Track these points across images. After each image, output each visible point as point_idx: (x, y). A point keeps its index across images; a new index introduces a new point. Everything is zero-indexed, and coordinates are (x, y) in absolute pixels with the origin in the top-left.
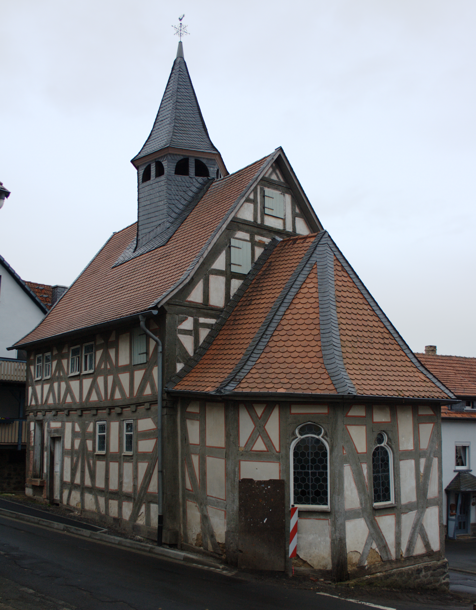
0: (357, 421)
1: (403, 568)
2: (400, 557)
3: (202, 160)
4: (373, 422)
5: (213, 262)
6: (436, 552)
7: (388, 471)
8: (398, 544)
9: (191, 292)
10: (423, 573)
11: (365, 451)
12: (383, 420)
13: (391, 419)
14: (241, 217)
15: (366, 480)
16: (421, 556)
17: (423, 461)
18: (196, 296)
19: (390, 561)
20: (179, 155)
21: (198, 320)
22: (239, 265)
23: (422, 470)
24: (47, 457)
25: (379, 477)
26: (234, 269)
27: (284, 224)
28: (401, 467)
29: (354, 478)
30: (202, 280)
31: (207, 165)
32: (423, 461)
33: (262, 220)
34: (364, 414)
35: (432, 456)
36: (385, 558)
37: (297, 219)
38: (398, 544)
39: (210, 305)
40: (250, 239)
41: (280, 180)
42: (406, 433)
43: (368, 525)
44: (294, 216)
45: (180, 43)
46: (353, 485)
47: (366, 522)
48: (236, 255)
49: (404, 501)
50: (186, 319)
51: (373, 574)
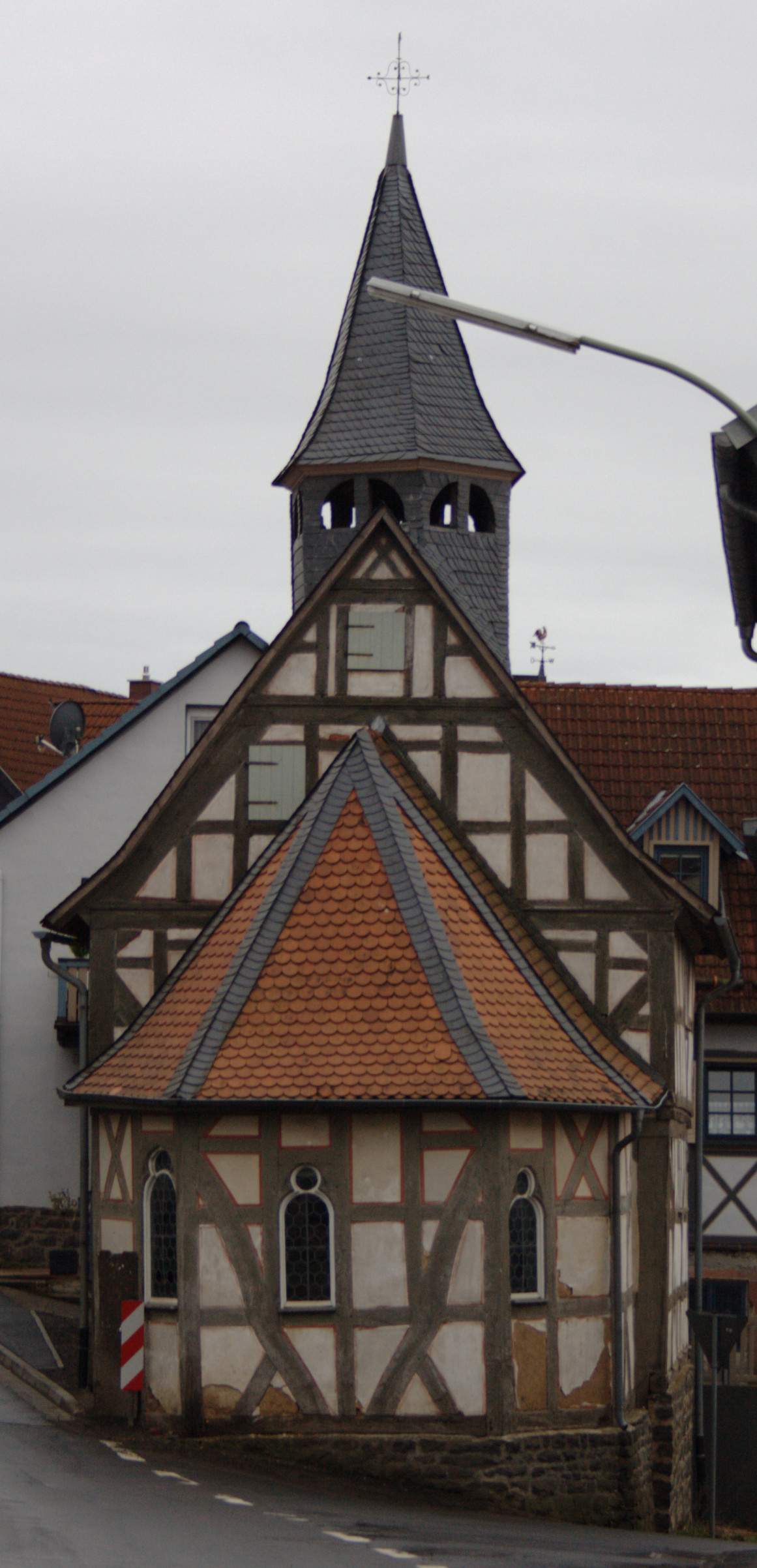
1: (361, 1436)
2: (354, 1413)
3: (385, 479)
4: (281, 1148)
5: (203, 806)
7: (326, 1241)
8: (346, 1385)
10: (418, 1452)
11: (255, 1200)
12: (309, 1143)
13: (544, 1142)
15: (260, 1257)
16: (421, 1421)
17: (430, 1230)
18: (160, 883)
19: (323, 1418)
20: (331, 476)
21: (165, 935)
22: (270, 803)
23: (427, 1244)
24: (627, 1334)
25: (304, 1254)
26: (256, 813)
27: (408, 682)
28: (353, 1236)
29: (227, 1251)
31: (398, 490)
32: (430, 1230)
33: (342, 684)
34: (253, 1131)
36: (309, 1408)
37: (450, 661)
38: (346, 1385)
39: (194, 901)
40: (306, 736)
41: (400, 574)
42: (375, 1169)
43: (261, 1341)
44: (441, 654)
45: (398, 118)
46: (225, 1263)
47: (257, 1334)
48: (260, 783)
49: (361, 1301)
50: (137, 935)
51: (272, 1433)
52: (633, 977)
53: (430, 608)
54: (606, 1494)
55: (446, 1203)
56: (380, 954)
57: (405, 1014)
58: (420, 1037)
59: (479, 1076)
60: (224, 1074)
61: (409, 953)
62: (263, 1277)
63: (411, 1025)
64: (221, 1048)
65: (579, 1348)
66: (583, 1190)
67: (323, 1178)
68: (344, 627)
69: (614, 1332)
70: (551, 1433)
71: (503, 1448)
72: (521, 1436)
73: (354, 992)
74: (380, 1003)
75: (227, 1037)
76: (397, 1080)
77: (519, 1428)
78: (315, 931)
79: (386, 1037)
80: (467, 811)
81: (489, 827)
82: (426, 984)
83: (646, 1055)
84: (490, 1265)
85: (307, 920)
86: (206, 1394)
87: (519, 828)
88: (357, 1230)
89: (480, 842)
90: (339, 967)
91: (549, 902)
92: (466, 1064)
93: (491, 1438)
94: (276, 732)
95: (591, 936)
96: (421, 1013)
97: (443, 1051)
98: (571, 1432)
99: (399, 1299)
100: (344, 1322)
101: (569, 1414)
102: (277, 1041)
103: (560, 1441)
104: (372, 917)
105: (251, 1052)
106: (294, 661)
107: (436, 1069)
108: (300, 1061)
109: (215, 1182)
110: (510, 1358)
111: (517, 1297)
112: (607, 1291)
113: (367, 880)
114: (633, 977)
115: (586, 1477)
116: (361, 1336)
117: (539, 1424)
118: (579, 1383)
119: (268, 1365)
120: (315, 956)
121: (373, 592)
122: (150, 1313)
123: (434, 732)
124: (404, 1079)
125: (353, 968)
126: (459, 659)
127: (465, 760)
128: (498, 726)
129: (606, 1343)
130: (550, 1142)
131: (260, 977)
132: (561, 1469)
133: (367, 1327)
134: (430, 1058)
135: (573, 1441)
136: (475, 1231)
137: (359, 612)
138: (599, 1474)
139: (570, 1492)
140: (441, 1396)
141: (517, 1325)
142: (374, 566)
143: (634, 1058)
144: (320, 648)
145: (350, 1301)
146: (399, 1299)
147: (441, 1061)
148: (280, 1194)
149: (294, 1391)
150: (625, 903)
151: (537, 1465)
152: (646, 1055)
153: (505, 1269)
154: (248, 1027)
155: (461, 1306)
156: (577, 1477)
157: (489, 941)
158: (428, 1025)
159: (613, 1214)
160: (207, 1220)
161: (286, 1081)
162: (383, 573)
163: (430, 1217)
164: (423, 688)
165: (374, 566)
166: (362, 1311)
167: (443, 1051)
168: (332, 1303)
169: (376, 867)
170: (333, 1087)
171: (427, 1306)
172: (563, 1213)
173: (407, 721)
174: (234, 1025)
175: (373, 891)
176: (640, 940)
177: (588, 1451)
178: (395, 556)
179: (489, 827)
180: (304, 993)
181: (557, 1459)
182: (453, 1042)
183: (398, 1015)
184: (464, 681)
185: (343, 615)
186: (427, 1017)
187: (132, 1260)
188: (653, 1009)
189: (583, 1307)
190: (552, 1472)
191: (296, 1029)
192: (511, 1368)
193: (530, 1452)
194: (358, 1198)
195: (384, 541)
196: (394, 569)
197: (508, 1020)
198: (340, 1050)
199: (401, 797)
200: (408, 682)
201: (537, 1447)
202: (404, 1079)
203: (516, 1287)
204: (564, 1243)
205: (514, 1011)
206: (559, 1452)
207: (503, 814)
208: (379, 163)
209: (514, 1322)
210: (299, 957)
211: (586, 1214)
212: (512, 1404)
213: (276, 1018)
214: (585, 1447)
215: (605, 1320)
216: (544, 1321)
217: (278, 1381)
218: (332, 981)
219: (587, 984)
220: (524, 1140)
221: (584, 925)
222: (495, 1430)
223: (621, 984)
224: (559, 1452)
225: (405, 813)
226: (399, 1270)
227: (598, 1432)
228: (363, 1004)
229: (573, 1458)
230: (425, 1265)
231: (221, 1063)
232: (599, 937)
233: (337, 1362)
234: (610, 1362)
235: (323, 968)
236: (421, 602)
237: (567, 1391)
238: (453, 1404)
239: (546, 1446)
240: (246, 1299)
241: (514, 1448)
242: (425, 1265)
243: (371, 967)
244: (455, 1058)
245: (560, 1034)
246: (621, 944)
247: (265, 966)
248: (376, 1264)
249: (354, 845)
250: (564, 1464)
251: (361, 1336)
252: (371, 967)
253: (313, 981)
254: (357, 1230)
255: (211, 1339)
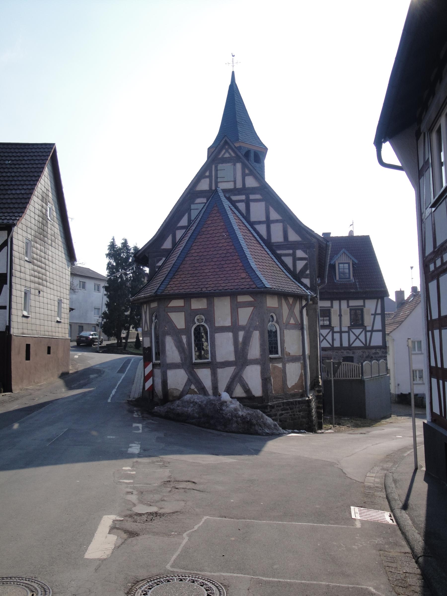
0: (177, 309)
6: (258, 398)
9: (164, 243)
14: (199, 189)
17: (241, 334)
23: (241, 339)
27: (235, 184)
29: (175, 344)
30: (171, 235)
32: (241, 334)
33: (216, 186)
34: (182, 304)
35: (251, 329)
43: (187, 374)
45: (233, 73)
46: (174, 348)
52: (304, 262)
53: (241, 163)
54: (304, 420)
55: (246, 325)
56: (223, 248)
57: (231, 265)
58: (236, 271)
59: (256, 282)
60: (172, 286)
61: (233, 247)
62: (187, 352)
63: (234, 268)
64: (171, 279)
65: (293, 373)
66: (292, 321)
67: (205, 319)
68: (217, 170)
69: (304, 367)
70: (285, 401)
71: (268, 407)
72: (275, 403)
73: (215, 260)
74: (223, 262)
75: (174, 275)
76: (228, 285)
77: (274, 400)
78: (203, 243)
79: (225, 272)
80: (253, 218)
81: (260, 223)
82: (238, 256)
83: (309, 285)
84: (262, 345)
85: (201, 240)
86: (169, 391)
87: (268, 222)
88: (217, 335)
89: (257, 227)
90: (210, 253)
91: (278, 242)
92: (251, 279)
93: (264, 404)
94: (199, 200)
95: (291, 252)
96: (236, 265)
97: (244, 275)
98: (292, 400)
99: (232, 358)
100: (214, 366)
101: (291, 394)
102: (190, 275)
103: (288, 404)
104: (221, 238)
105: (181, 279)
106: (203, 181)
107: (241, 281)
108: (197, 281)
109: (170, 321)
110: (270, 376)
111: (271, 356)
112: (301, 354)
113: (219, 227)
114: (304, 262)
115: (297, 415)
116: (219, 371)
117: (281, 398)
118: (293, 384)
119: (189, 382)
120: (203, 250)
121: (224, 161)
122: (154, 366)
123: (243, 197)
124: (230, 284)
125: (215, 253)
126: (249, 177)
127: (252, 204)
128: (261, 194)
129: (302, 370)
130: (280, 305)
131: (185, 257)
132: (289, 413)
133: (221, 368)
134: (239, 278)
135: (292, 403)
136: (256, 335)
137: (220, 166)
138: (301, 413)
139: (292, 420)
140: (247, 390)
141: (272, 366)
142: (224, 154)
143: (305, 286)
144: (210, 177)
145: (215, 359)
146: (232, 358)
147: (243, 278)
148: (192, 325)
149: (198, 390)
150: (300, 241)
151: (280, 412)
152: (309, 285)
153: (267, 347)
154: (181, 272)
155: (252, 360)
156: (294, 415)
157: (259, 246)
158: (239, 268)
159: (302, 329)
160: (168, 334)
161: (191, 287)
162: (227, 155)
163: (241, 330)
164: (239, 185)
165: (224, 154)
166: (219, 363)
167: (244, 275)
168: (210, 360)
169: (222, 224)
170: (207, 288)
171: (241, 360)
172: (286, 328)
173: (235, 195)
174: (176, 271)
175: (222, 230)
176: (305, 252)
177: (297, 406)
178: (230, 151)
179: (260, 223)
180: (199, 261)
181: (287, 409)
182: (247, 272)
183: (229, 265)
184: (251, 182)
185: (216, 167)
186: (238, 265)
187: (150, 349)
188: (310, 272)
189: (294, 359)
190: (286, 414)
191: (197, 272)
192: (270, 380)
193: (278, 408)
194: (217, 325)
195: (227, 147)
196: (230, 154)
197: (265, 267)
198: (210, 277)
199: (230, 205)
200: (235, 184)
201: (281, 406)
202: (230, 284)
203: (271, 353)
204: (287, 339)
205: (267, 265)
206: (288, 407)
207: (264, 219)
208: (229, 83)
209: (271, 364)
210: (198, 251)
211: (293, 329)
212: (271, 392)
213: (190, 269)
214: (296, 405)
215: (301, 363)
216: (281, 364)
217: (193, 387)
218: (208, 257)
219: (290, 266)
220: (272, 302)
221: (289, 249)
222: (266, 401)
223: (300, 265)
224: (288, 407)
225: (231, 209)
226: (231, 348)
227: (300, 399)
228: (218, 263)
229: (293, 409)
230: (240, 346)
231: (172, 283)
232: (293, 252)
233: (212, 380)
234: (303, 377)
235: (205, 254)
236: (237, 162)
237: (289, 387)
238: (251, 393)
239: (283, 406)
240: (182, 360)
241: (272, 407)
242: (240, 346)
243: (220, 252)
244: (247, 277)
245: (282, 273)
246: (300, 253)
247: (187, 254)
248: (224, 347)
249: (216, 218)
250: (290, 411)
251: (219, 371)
252: (220, 252)
253: (202, 258)
254: (217, 335)
255: (170, 373)
